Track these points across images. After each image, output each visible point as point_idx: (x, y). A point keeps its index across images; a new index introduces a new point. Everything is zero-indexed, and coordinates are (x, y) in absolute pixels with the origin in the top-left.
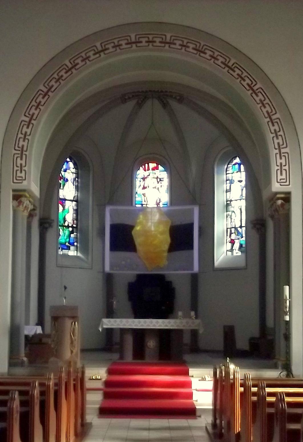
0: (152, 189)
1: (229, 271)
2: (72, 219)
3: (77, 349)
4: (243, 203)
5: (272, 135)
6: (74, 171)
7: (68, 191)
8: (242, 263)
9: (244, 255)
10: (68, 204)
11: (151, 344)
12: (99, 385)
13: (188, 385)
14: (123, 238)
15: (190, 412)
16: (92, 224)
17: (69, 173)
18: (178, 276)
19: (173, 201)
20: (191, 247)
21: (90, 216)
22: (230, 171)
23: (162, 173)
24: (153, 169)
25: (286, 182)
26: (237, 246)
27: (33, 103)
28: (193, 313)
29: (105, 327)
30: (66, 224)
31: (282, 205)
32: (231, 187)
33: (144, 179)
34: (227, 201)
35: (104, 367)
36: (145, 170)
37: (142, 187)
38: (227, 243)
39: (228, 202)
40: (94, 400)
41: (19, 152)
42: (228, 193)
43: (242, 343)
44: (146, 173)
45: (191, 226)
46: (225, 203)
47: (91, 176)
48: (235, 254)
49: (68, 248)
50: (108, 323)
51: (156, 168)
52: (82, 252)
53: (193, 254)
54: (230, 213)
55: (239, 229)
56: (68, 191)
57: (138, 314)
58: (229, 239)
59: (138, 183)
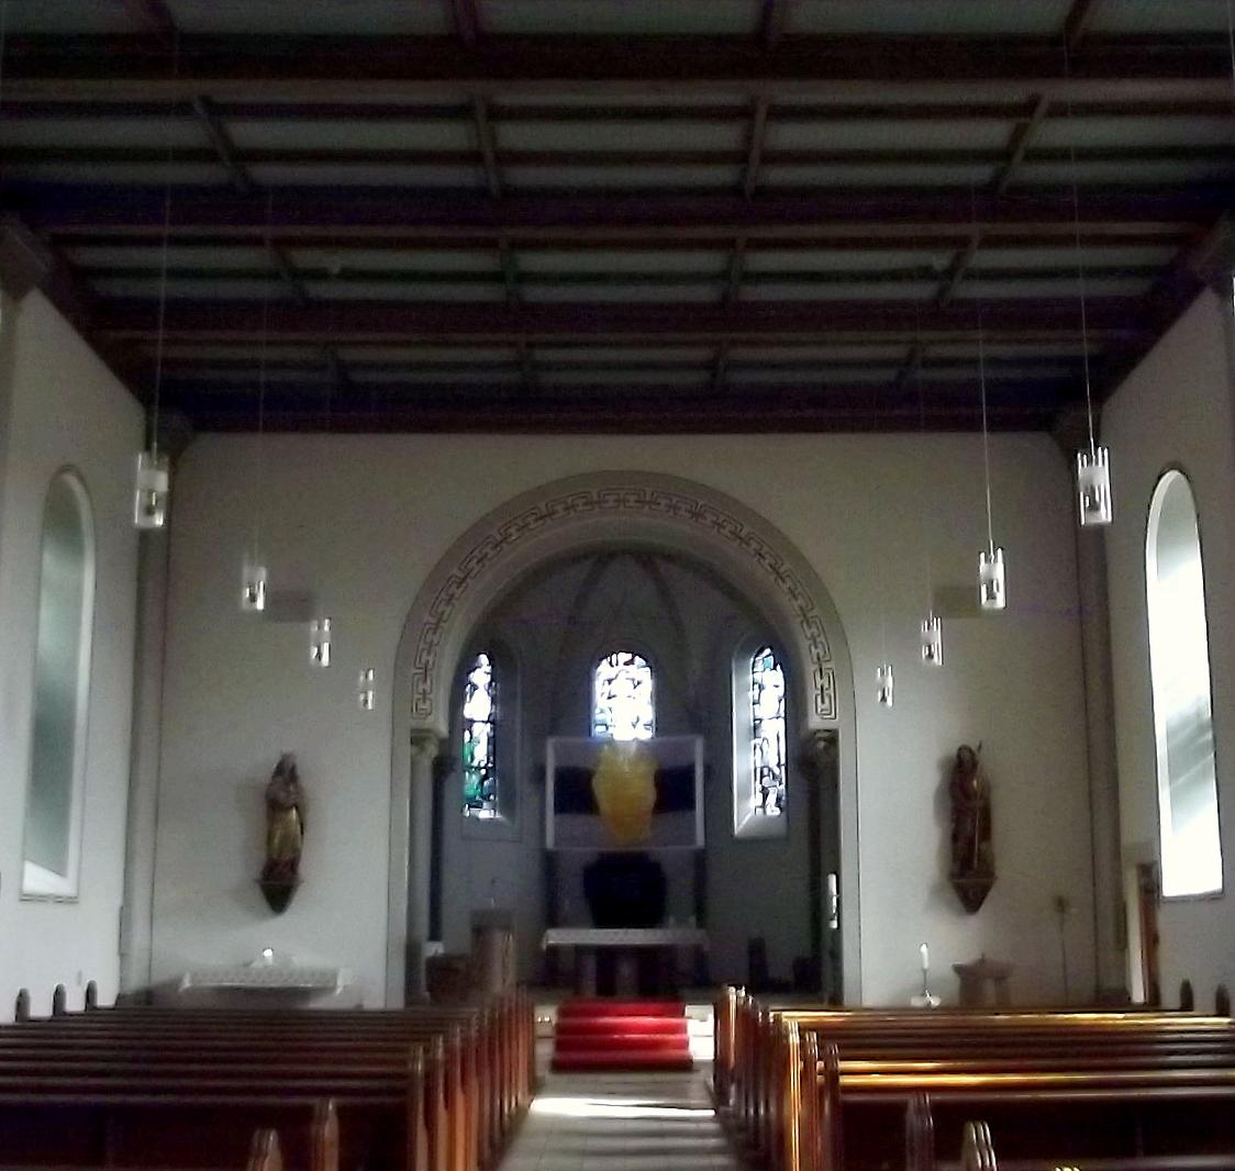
0: (624, 702)
1: (756, 843)
2: (485, 752)
3: (511, 978)
4: (780, 725)
5: (808, 642)
6: (489, 669)
7: (478, 706)
8: (780, 828)
9: (784, 813)
10: (477, 728)
11: (626, 970)
12: (548, 1031)
13: (682, 1029)
14: (576, 791)
15: (686, 1065)
16: (520, 767)
17: (481, 676)
18: (670, 854)
19: (661, 724)
20: (691, 805)
21: (518, 748)
22: (759, 666)
23: (641, 672)
24: (626, 664)
25: (830, 714)
26: (772, 799)
27: (443, 595)
28: (692, 920)
29: (551, 942)
30: (475, 763)
31: (825, 748)
32: (760, 695)
33: (610, 681)
34: (755, 720)
35: (555, 1004)
36: (612, 666)
37: (606, 695)
38: (761, 778)
39: (757, 722)
40: (545, 1051)
41: (421, 671)
42: (756, 706)
43: (780, 968)
44: (616, 669)
45: (690, 770)
46: (752, 724)
47: (519, 678)
48: (769, 813)
49: (479, 806)
50: (555, 937)
51: (631, 662)
52: (501, 813)
53: (694, 816)
54: (758, 741)
55: (777, 771)
56: (478, 706)
57: (602, 921)
58: (759, 787)
59: (600, 688)
